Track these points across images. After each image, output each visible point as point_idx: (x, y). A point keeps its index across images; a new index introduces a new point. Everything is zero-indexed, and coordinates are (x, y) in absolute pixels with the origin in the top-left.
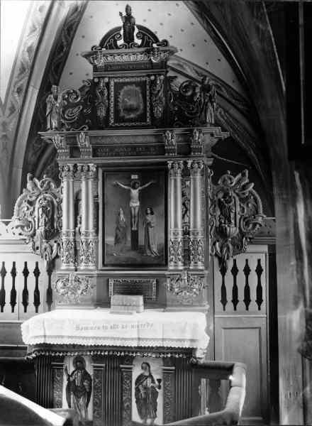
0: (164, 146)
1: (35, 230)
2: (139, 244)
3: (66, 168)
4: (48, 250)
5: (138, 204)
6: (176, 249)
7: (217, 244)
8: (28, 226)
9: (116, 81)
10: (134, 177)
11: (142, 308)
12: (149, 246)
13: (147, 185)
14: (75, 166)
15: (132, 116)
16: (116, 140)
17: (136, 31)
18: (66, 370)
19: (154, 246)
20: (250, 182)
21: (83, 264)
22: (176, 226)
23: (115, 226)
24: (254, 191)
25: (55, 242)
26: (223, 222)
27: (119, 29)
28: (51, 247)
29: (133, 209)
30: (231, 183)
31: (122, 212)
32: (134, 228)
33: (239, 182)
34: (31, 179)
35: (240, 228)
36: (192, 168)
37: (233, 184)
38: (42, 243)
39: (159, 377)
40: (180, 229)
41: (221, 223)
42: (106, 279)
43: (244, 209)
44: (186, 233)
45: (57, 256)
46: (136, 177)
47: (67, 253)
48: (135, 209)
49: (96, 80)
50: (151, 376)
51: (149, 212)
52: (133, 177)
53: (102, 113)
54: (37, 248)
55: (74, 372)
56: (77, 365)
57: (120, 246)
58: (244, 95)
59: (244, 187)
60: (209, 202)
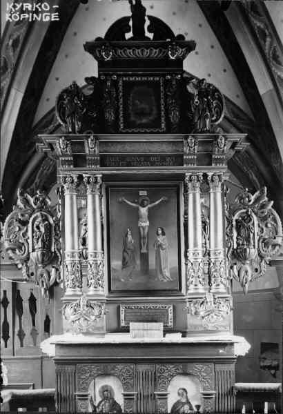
0: (182, 156)
1: (29, 253)
2: (150, 268)
3: (68, 179)
4: (45, 275)
5: (148, 223)
6: (196, 271)
7: (235, 267)
8: (20, 248)
9: (124, 79)
10: (143, 193)
11: (56, 397)
12: (161, 270)
13: (157, 202)
14: (80, 177)
15: (144, 121)
16: (128, 148)
17: (147, 23)
18: (91, 401)
19: (165, 270)
20: (269, 201)
21: (92, 288)
22: (195, 245)
23: (122, 248)
24: (273, 210)
25: (53, 267)
26: (241, 243)
27: (126, 19)
28: (49, 273)
29: (141, 229)
30: (250, 201)
31: (129, 233)
32: (144, 251)
33: (257, 200)
34: (22, 194)
35: (259, 250)
36: (212, 181)
37: (251, 203)
38: (37, 268)
39: (197, 403)
40: (200, 249)
41: (238, 245)
42: (117, 305)
43: (262, 229)
44: (207, 253)
45: (56, 284)
46: (145, 193)
47: (73, 276)
48: (144, 229)
49: (103, 78)
50: (188, 402)
51: (160, 232)
52: (141, 193)
53: (110, 116)
54: (32, 274)
55: (100, 402)
56: (103, 394)
57: (125, 271)
58: (252, 117)
59: (263, 206)
60: (226, 221)
